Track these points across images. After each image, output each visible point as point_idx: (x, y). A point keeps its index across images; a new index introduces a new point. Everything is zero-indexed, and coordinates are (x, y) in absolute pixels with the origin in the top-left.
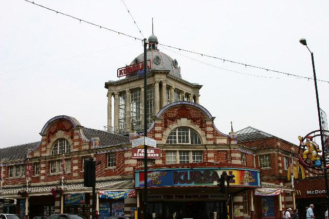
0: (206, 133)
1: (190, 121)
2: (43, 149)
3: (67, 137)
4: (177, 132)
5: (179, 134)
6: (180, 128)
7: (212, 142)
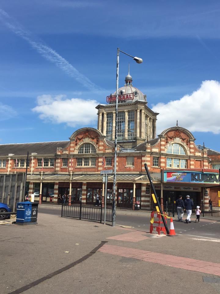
0: (190, 148)
5: (85, 149)
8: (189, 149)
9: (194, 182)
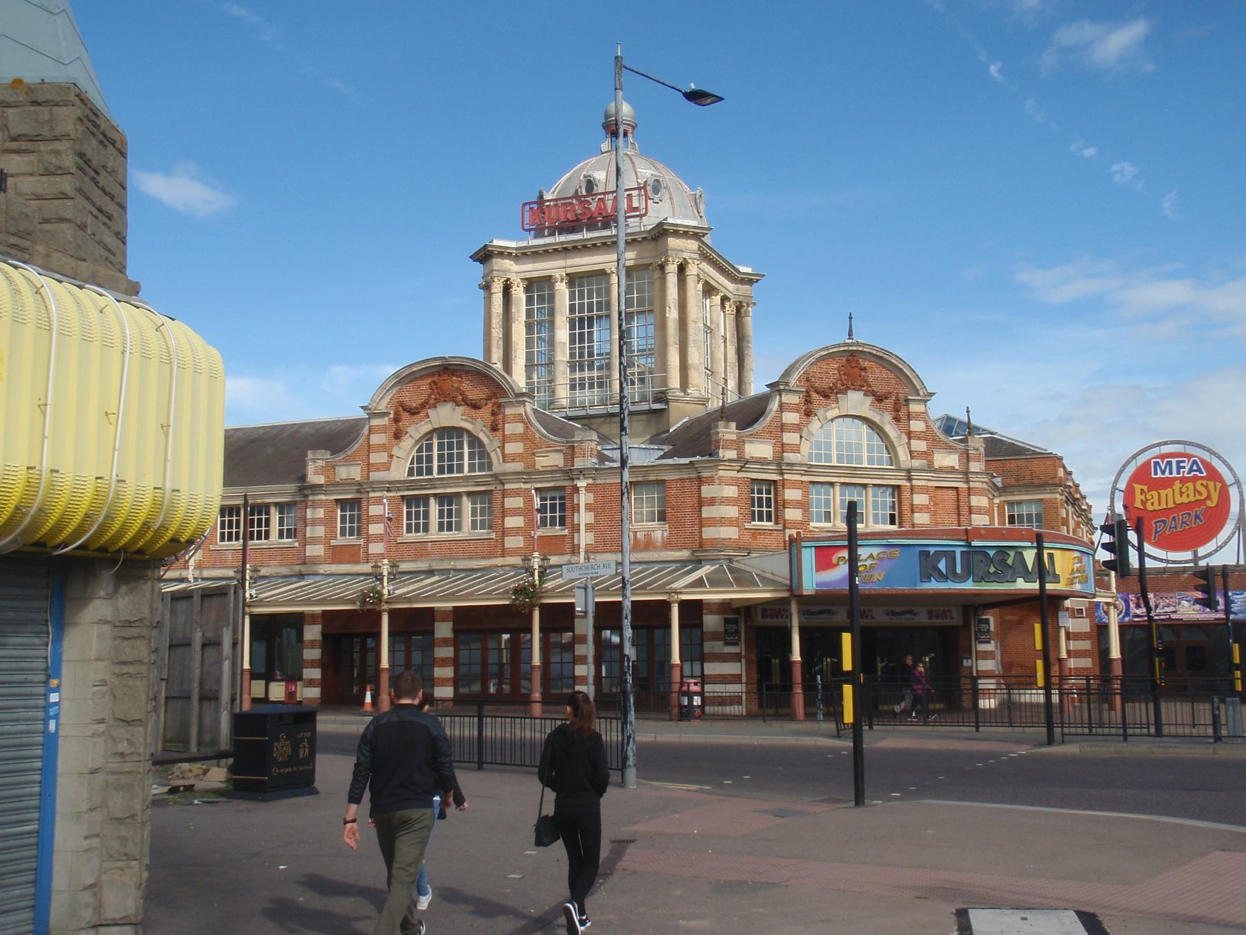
1: (460, 410)
2: (376, 458)
3: (477, 425)
4: (435, 442)
5: (441, 447)
6: (443, 432)
7: (518, 466)
8: (905, 438)
9: (934, 585)
